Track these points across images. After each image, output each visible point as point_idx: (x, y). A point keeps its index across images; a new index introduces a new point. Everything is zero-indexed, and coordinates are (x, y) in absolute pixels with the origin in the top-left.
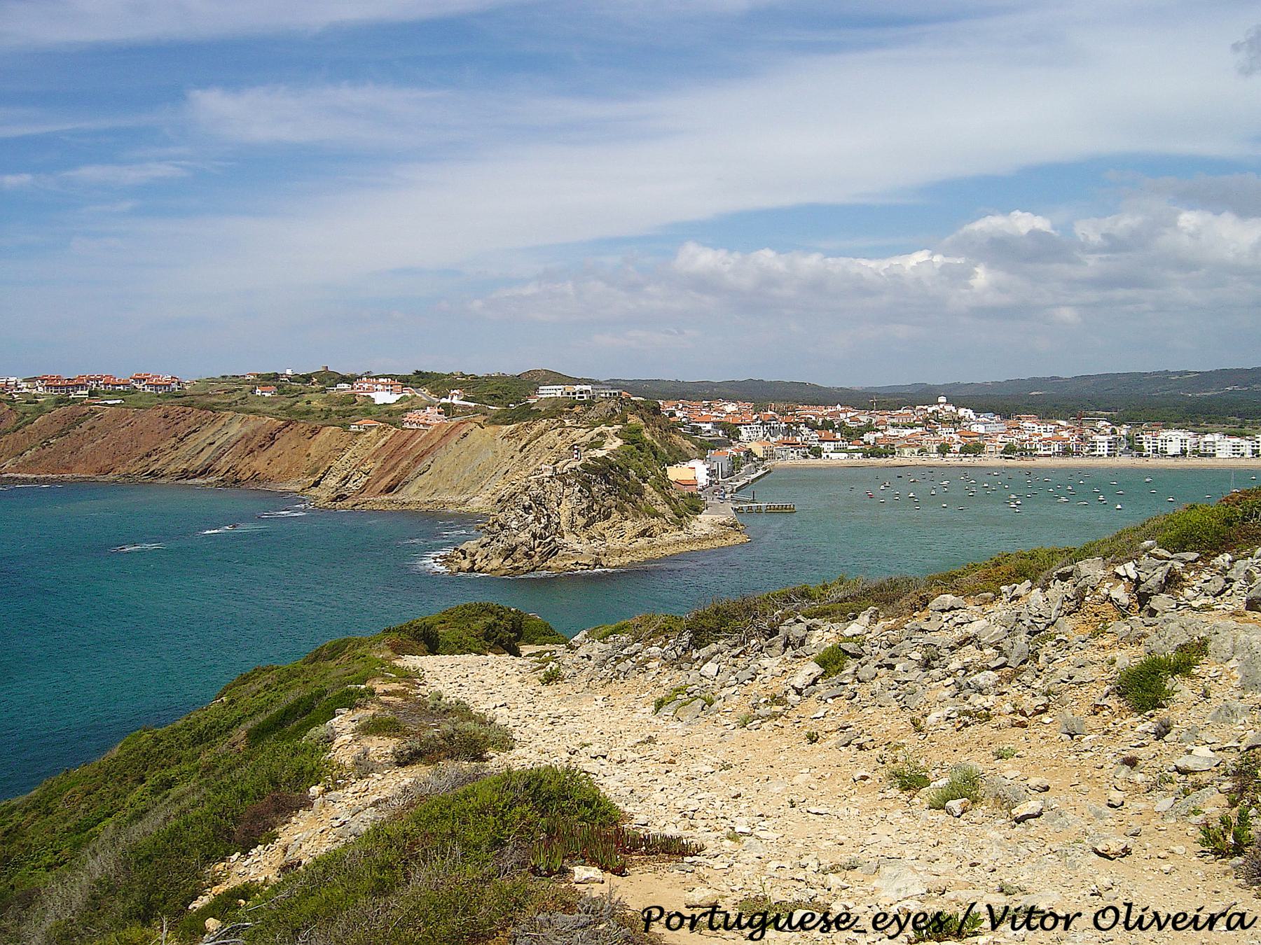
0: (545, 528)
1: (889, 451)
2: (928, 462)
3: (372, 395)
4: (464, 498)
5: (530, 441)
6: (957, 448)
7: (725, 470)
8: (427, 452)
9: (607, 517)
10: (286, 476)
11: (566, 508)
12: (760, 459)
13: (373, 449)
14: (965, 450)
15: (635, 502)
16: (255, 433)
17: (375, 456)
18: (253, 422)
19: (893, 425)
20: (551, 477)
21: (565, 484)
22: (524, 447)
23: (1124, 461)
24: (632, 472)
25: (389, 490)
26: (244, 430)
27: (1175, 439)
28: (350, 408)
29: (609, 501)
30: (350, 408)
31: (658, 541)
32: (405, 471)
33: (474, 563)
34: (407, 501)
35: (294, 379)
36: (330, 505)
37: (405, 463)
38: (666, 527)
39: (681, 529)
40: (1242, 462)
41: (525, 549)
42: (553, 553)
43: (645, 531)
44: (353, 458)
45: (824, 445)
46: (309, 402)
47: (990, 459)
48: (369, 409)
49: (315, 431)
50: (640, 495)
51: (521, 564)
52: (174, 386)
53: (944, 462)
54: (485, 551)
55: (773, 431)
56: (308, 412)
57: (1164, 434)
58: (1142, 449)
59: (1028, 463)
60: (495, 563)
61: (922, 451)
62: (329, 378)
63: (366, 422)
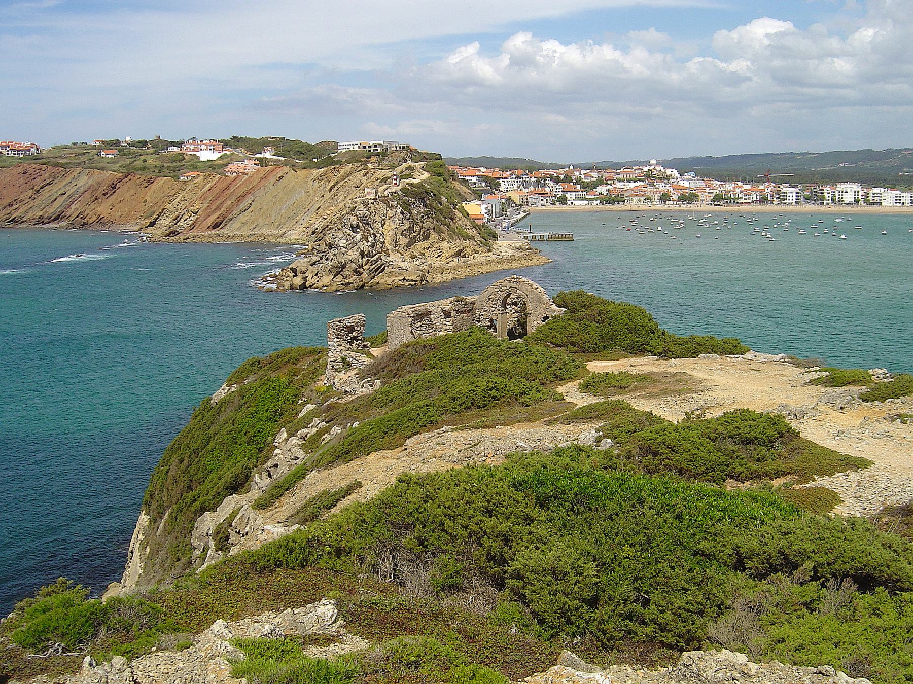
0: (373, 246)
1: (619, 198)
2: (653, 208)
3: (198, 154)
4: (281, 231)
5: (337, 182)
6: (675, 197)
7: (497, 211)
8: (248, 193)
9: (426, 238)
10: (126, 218)
11: (390, 228)
12: (517, 205)
13: (200, 193)
14: (682, 198)
15: (448, 226)
16: (99, 184)
17: (203, 198)
18: (98, 176)
19: (619, 180)
20: (375, 199)
21: (388, 206)
22: (333, 187)
23: (810, 207)
24: (443, 199)
25: (216, 226)
26: (90, 182)
27: (850, 191)
28: (179, 164)
29: (428, 223)
30: (179, 164)
31: (471, 261)
32: (229, 210)
33: (305, 279)
34: (231, 235)
35: (132, 144)
36: (163, 239)
37: (229, 203)
38: (477, 248)
39: (489, 251)
40: (904, 209)
41: (354, 266)
42: (380, 270)
43: (460, 251)
44: (185, 201)
45: (568, 195)
46: (145, 161)
47: (703, 206)
48: (195, 164)
49: (150, 181)
50: (452, 219)
51: (351, 280)
52: (33, 150)
53: (666, 208)
54: (315, 269)
55: (526, 184)
56: (144, 168)
57: (841, 187)
58: (823, 198)
59: (732, 208)
60: (326, 280)
61: (648, 199)
62: (160, 145)
63: (195, 174)
